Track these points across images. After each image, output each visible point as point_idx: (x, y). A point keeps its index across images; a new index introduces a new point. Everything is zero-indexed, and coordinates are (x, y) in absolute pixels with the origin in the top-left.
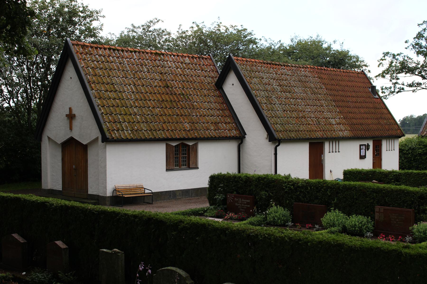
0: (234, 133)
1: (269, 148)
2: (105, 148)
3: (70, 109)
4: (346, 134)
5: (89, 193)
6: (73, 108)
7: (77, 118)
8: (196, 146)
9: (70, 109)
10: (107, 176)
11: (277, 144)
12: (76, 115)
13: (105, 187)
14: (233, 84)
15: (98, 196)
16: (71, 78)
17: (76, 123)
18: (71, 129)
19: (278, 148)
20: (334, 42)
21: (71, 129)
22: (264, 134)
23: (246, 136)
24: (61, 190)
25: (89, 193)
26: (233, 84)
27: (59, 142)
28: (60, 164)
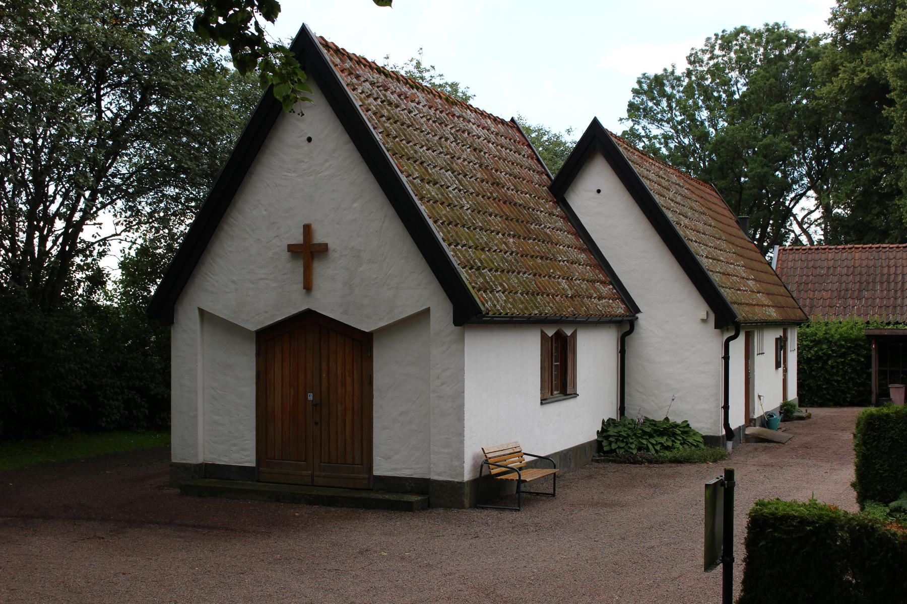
0: (619, 309)
1: (709, 341)
2: (462, 340)
3: (307, 230)
4: (773, 314)
5: (376, 472)
6: (315, 227)
7: (332, 255)
8: (574, 335)
9: (307, 230)
10: (467, 423)
11: (733, 334)
12: (331, 246)
13: (460, 456)
14: (599, 191)
15: (428, 481)
16: (309, 140)
17: (323, 272)
18: (308, 287)
19: (731, 343)
20: (569, 131)
21: (308, 287)
22: (699, 309)
23: (637, 315)
24: (254, 465)
25: (376, 472)
26: (599, 191)
27: (253, 327)
28: (250, 391)
